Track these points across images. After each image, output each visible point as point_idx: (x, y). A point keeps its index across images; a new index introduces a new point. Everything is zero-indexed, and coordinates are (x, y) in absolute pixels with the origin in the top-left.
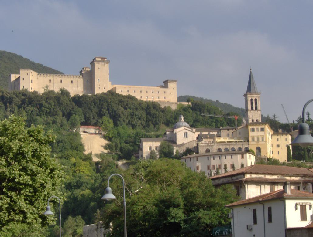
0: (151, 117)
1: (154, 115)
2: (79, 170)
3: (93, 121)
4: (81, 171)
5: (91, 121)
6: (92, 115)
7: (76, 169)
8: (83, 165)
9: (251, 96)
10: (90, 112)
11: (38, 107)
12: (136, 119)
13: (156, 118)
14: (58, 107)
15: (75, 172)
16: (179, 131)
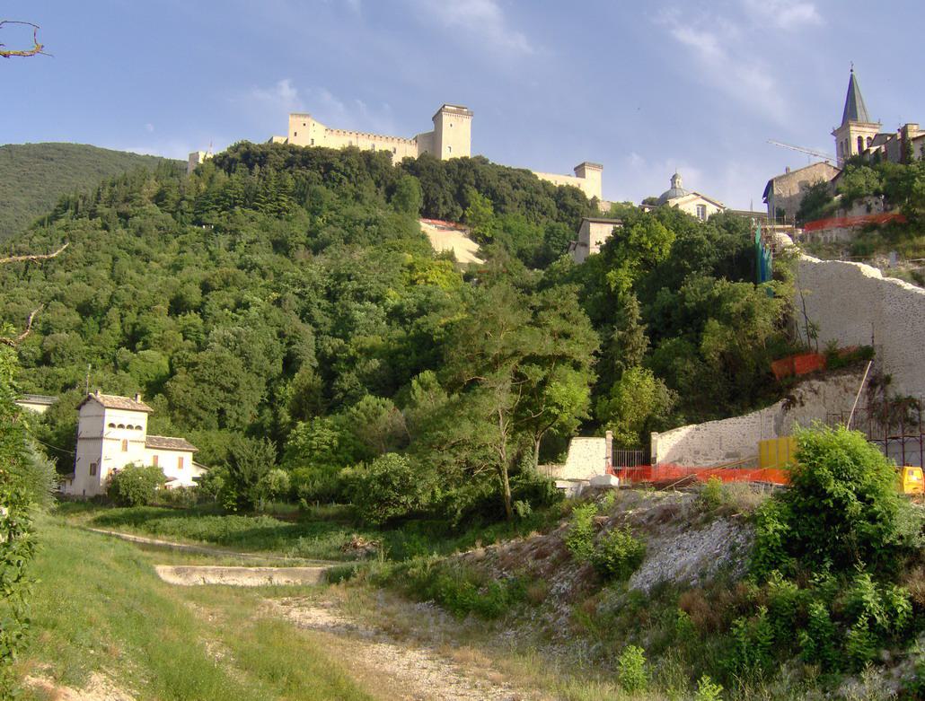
0: (568, 214)
1: (573, 209)
2: (426, 278)
3: (444, 210)
4: (429, 280)
5: (439, 208)
6: (441, 196)
7: (416, 277)
8: (437, 268)
9: (859, 129)
10: (438, 189)
11: (322, 171)
12: (537, 213)
13: (577, 215)
14: (366, 173)
15: (413, 282)
16: (686, 202)
